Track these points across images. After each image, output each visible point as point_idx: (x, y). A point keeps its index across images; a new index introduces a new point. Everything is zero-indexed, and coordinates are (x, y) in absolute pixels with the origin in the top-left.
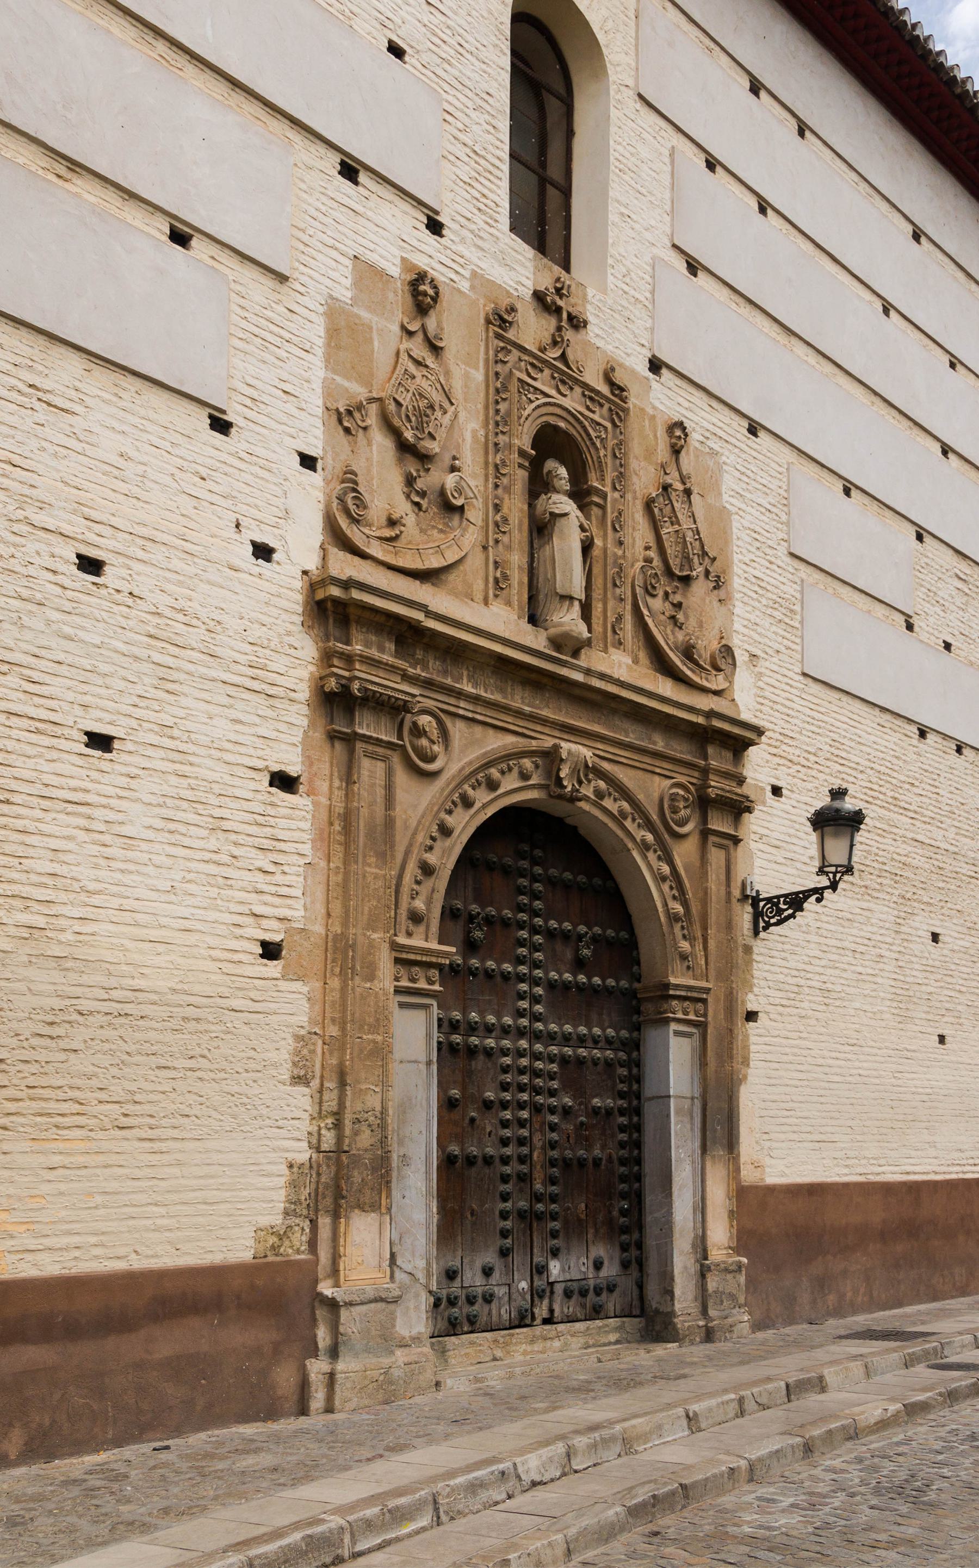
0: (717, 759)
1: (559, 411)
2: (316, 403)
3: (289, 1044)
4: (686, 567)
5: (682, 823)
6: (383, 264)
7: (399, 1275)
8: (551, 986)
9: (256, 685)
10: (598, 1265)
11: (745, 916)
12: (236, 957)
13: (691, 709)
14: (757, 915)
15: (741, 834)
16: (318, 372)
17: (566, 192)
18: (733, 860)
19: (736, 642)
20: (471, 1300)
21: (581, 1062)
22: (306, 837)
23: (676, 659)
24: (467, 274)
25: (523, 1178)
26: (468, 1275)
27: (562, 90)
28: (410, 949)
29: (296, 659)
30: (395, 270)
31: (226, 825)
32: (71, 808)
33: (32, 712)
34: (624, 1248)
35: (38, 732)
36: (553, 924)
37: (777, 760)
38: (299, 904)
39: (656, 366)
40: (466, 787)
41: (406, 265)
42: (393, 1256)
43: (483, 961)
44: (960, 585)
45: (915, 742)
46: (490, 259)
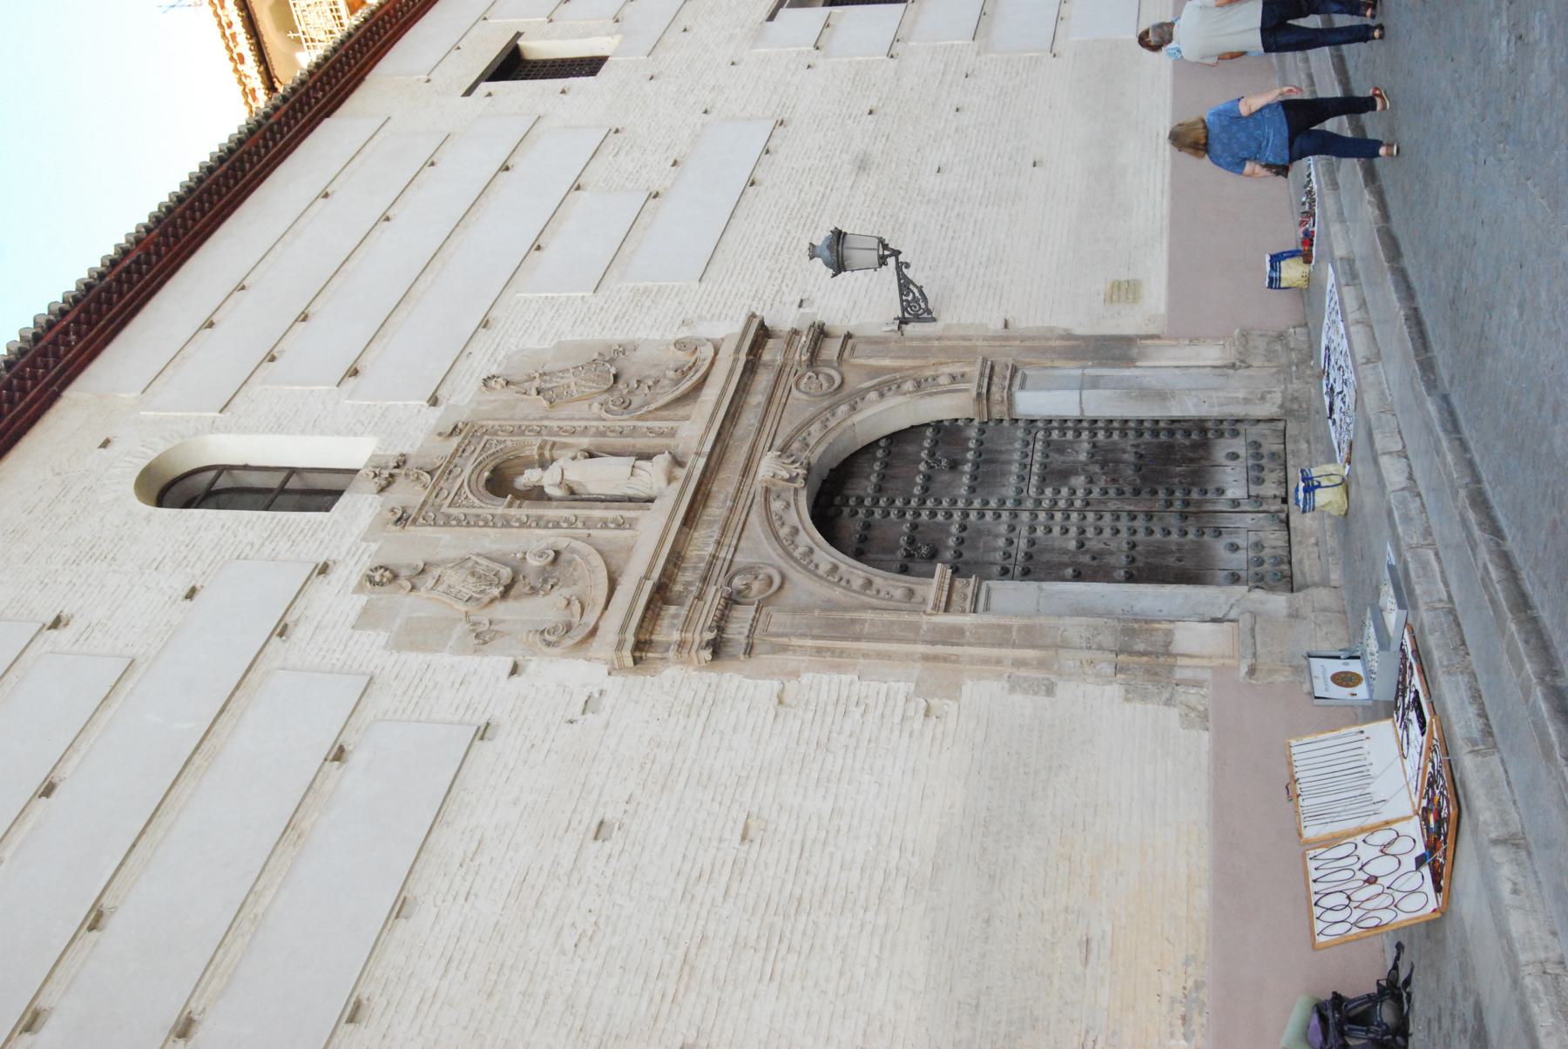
0: (772, 353)
1: (474, 477)
2: (471, 662)
3: (1018, 698)
4: (612, 373)
5: (831, 379)
6: (358, 608)
7: (1233, 615)
8: (972, 490)
9: (705, 713)
10: (1234, 456)
11: (912, 329)
12: (939, 736)
13: (732, 371)
15: (843, 333)
16: (445, 659)
17: (293, 471)
19: (671, 337)
20: (1260, 562)
21: (1044, 466)
22: (835, 677)
23: (686, 385)
24: (364, 544)
25: (1149, 516)
26: (1233, 566)
27: (213, 473)
28: (937, 599)
29: (680, 679)
30: (363, 599)
31: (824, 740)
32: (806, 854)
33: (725, 878)
34: (1220, 434)
35: (742, 874)
36: (917, 490)
37: (776, 303)
38: (894, 686)
39: (434, 401)
40: (797, 554)
41: (359, 589)
42: (1214, 620)
43: (948, 548)
44: (623, 153)
45: (762, 188)
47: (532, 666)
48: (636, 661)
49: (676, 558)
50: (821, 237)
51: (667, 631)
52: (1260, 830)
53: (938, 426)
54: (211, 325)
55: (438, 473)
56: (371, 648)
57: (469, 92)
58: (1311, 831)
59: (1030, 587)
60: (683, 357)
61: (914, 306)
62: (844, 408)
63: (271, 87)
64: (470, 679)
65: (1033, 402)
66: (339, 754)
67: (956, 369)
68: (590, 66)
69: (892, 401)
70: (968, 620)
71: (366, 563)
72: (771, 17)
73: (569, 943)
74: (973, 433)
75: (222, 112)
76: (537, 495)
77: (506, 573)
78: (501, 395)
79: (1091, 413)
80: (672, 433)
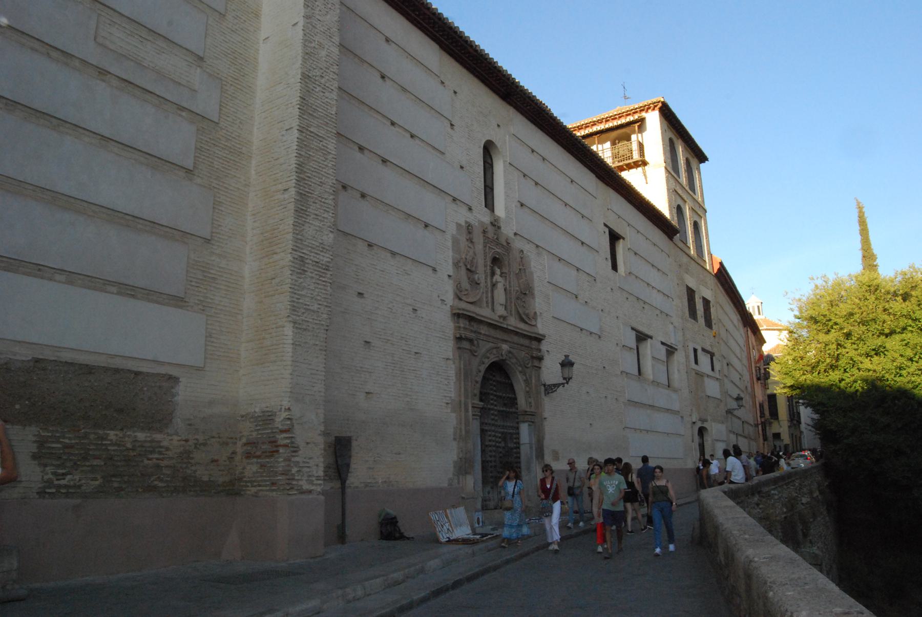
0: (534, 344)
4: (526, 292)
11: (543, 387)
14: (546, 390)
16: (450, 253)
23: (524, 317)
25: (495, 466)
29: (449, 327)
30: (463, 224)
39: (515, 234)
41: (466, 222)
46: (481, 216)
48: (455, 314)
49: (480, 322)
50: (571, 358)
51: (463, 323)
52: (444, 498)
53: (516, 399)
54: (383, 77)
55: (497, 241)
56: (452, 230)
57: (605, 225)
58: (448, 511)
59: (478, 432)
60: (532, 314)
61: (550, 389)
62: (520, 369)
63: (584, 137)
64: (446, 261)
65: (524, 429)
66: (426, 226)
67: (533, 404)
68: (615, 267)
69: (523, 385)
70: (470, 413)
71: (473, 223)
72: (633, 329)
74: (514, 410)
75: (572, 116)
76: (493, 274)
77: (473, 269)
79: (522, 447)
80: (511, 315)
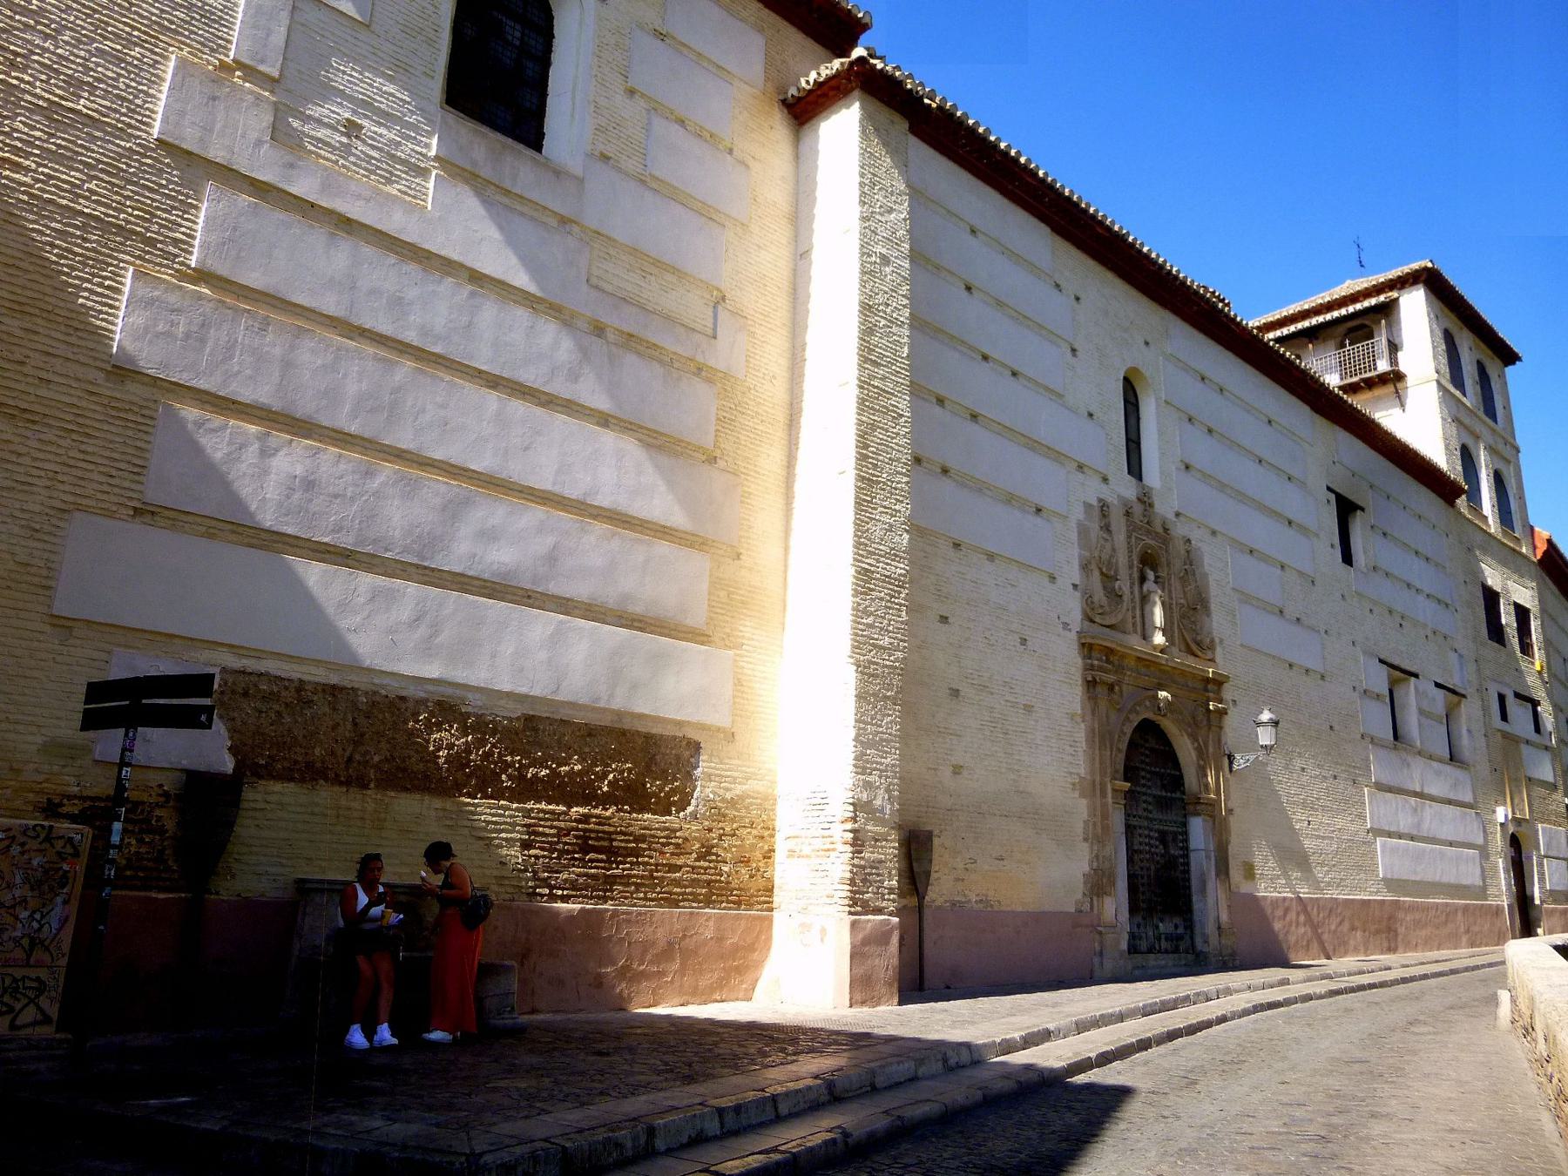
3: (1082, 825)
10: (1176, 927)
18: (1444, 360)
23: (1194, 647)
39: (1178, 515)
41: (1100, 500)
46: (1125, 488)
47: (1078, 594)
53: (1181, 777)
56: (1078, 513)
68: (1347, 558)
69: (1194, 755)
71: (1109, 500)
72: (1381, 661)
73: (987, 634)
74: (1178, 795)
76: (1143, 579)
78: (1182, 548)
79: (1192, 855)
